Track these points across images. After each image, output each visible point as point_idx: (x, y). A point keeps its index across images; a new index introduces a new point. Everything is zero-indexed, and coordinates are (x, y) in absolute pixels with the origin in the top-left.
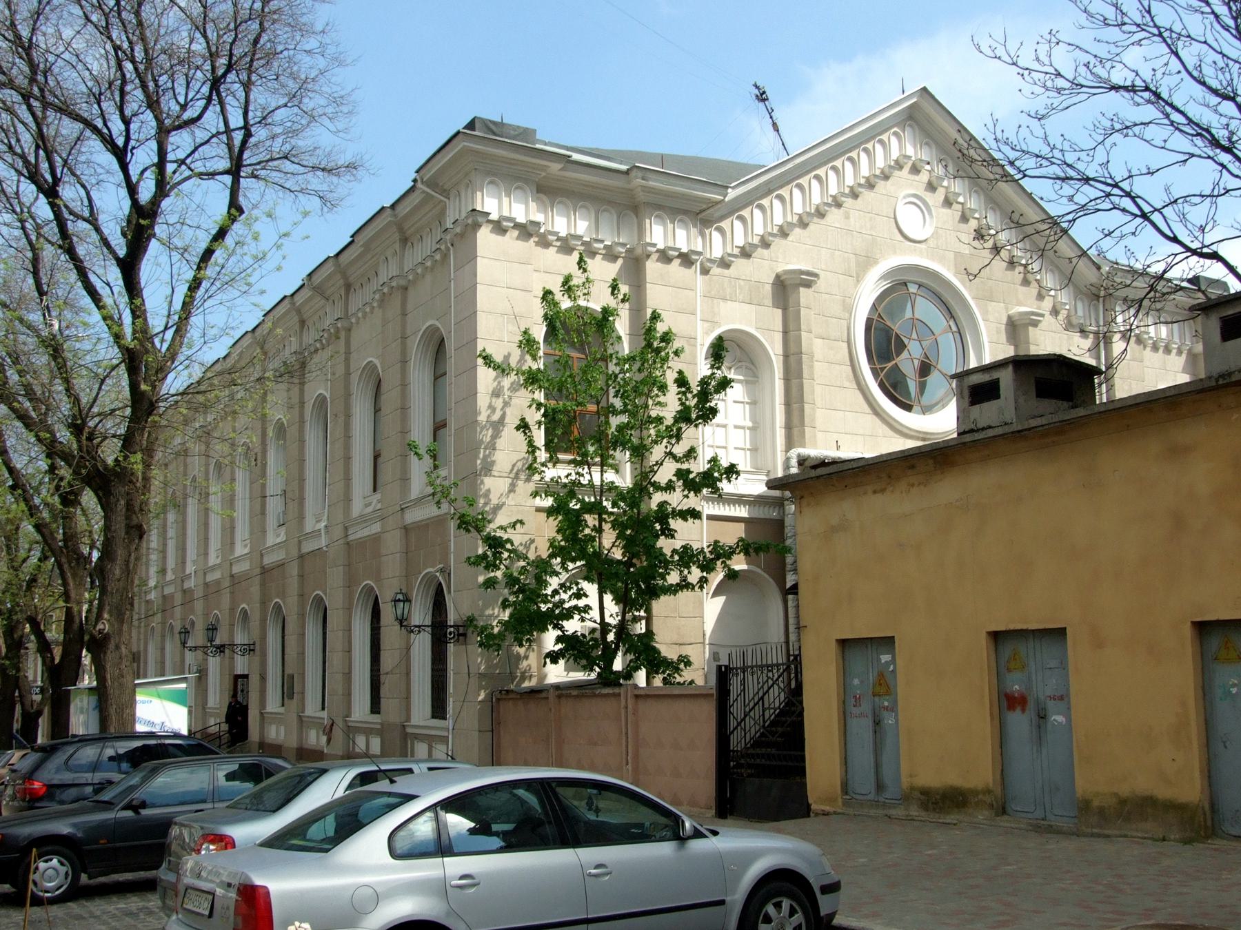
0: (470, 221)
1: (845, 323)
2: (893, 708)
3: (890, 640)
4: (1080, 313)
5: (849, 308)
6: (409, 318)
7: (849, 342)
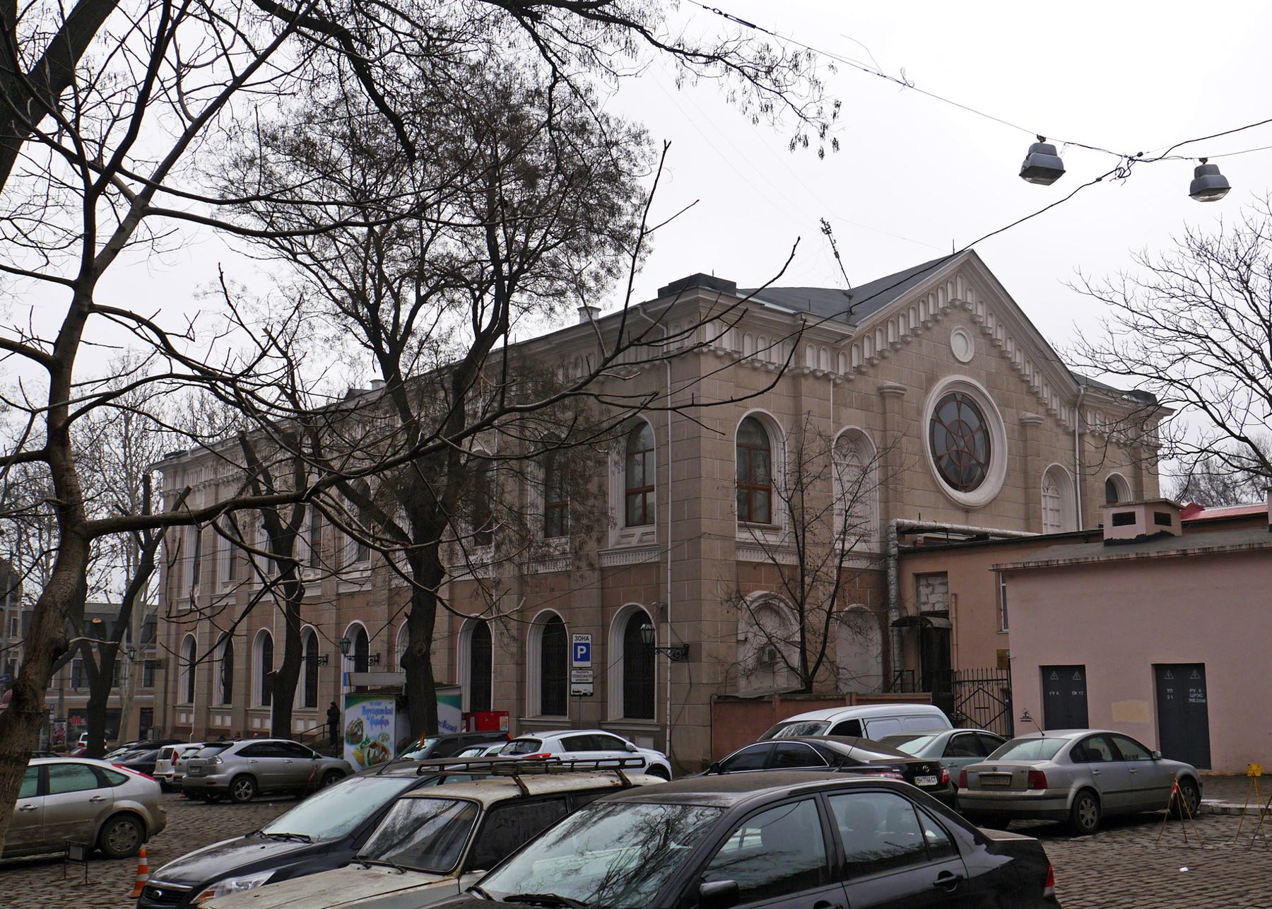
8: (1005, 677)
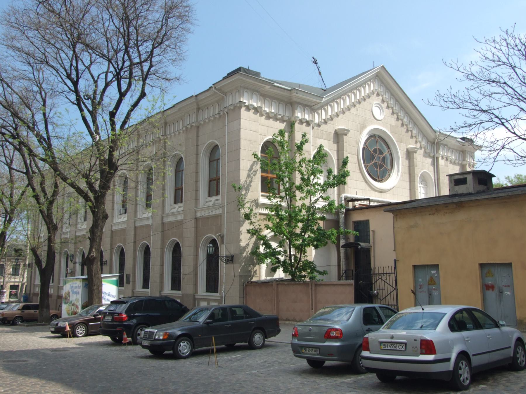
0: (238, 105)
1: (356, 149)
2: (438, 289)
3: (437, 266)
4: (429, 148)
5: (358, 143)
6: (200, 138)
7: (358, 156)
8: (393, 272)
